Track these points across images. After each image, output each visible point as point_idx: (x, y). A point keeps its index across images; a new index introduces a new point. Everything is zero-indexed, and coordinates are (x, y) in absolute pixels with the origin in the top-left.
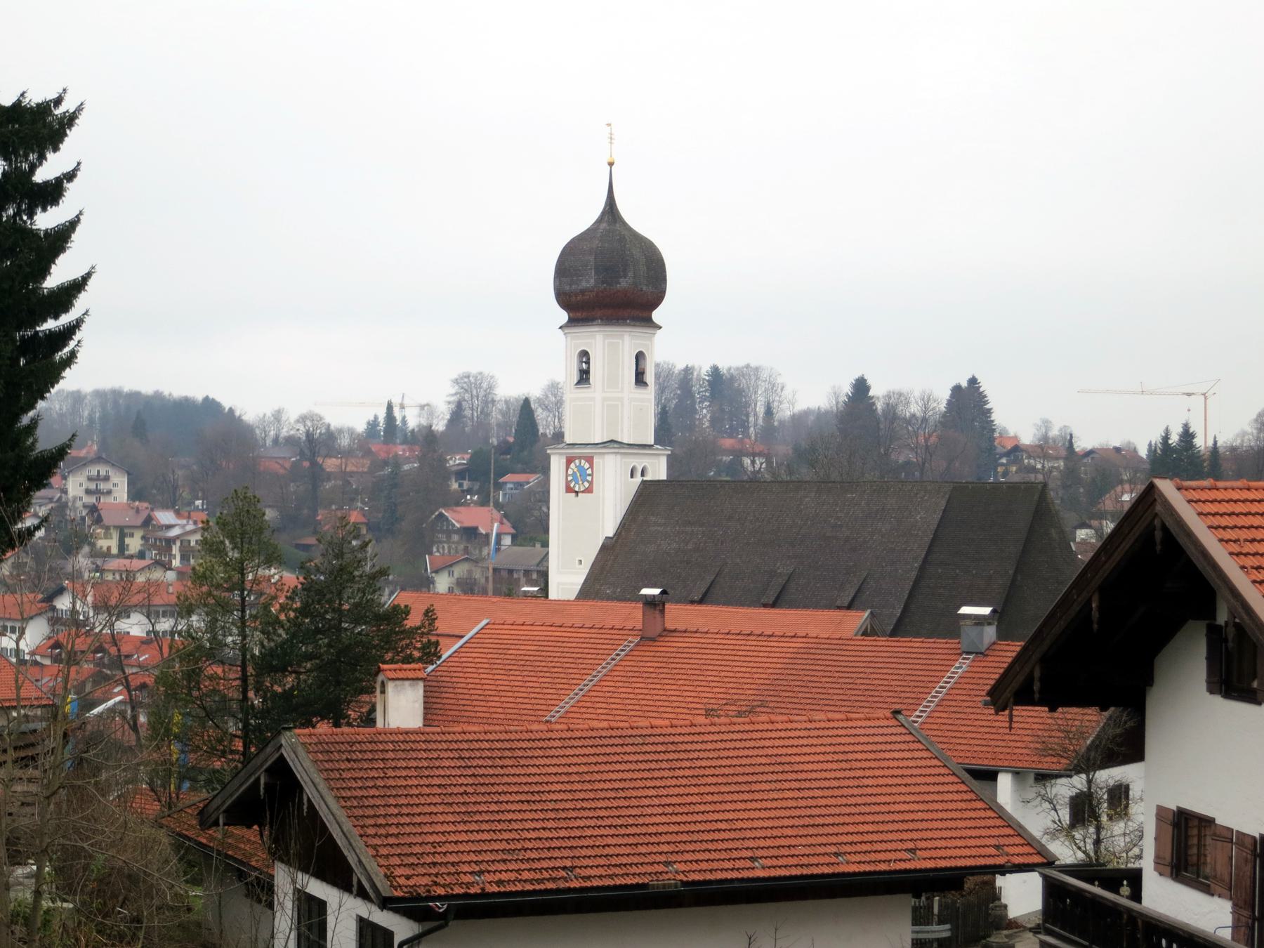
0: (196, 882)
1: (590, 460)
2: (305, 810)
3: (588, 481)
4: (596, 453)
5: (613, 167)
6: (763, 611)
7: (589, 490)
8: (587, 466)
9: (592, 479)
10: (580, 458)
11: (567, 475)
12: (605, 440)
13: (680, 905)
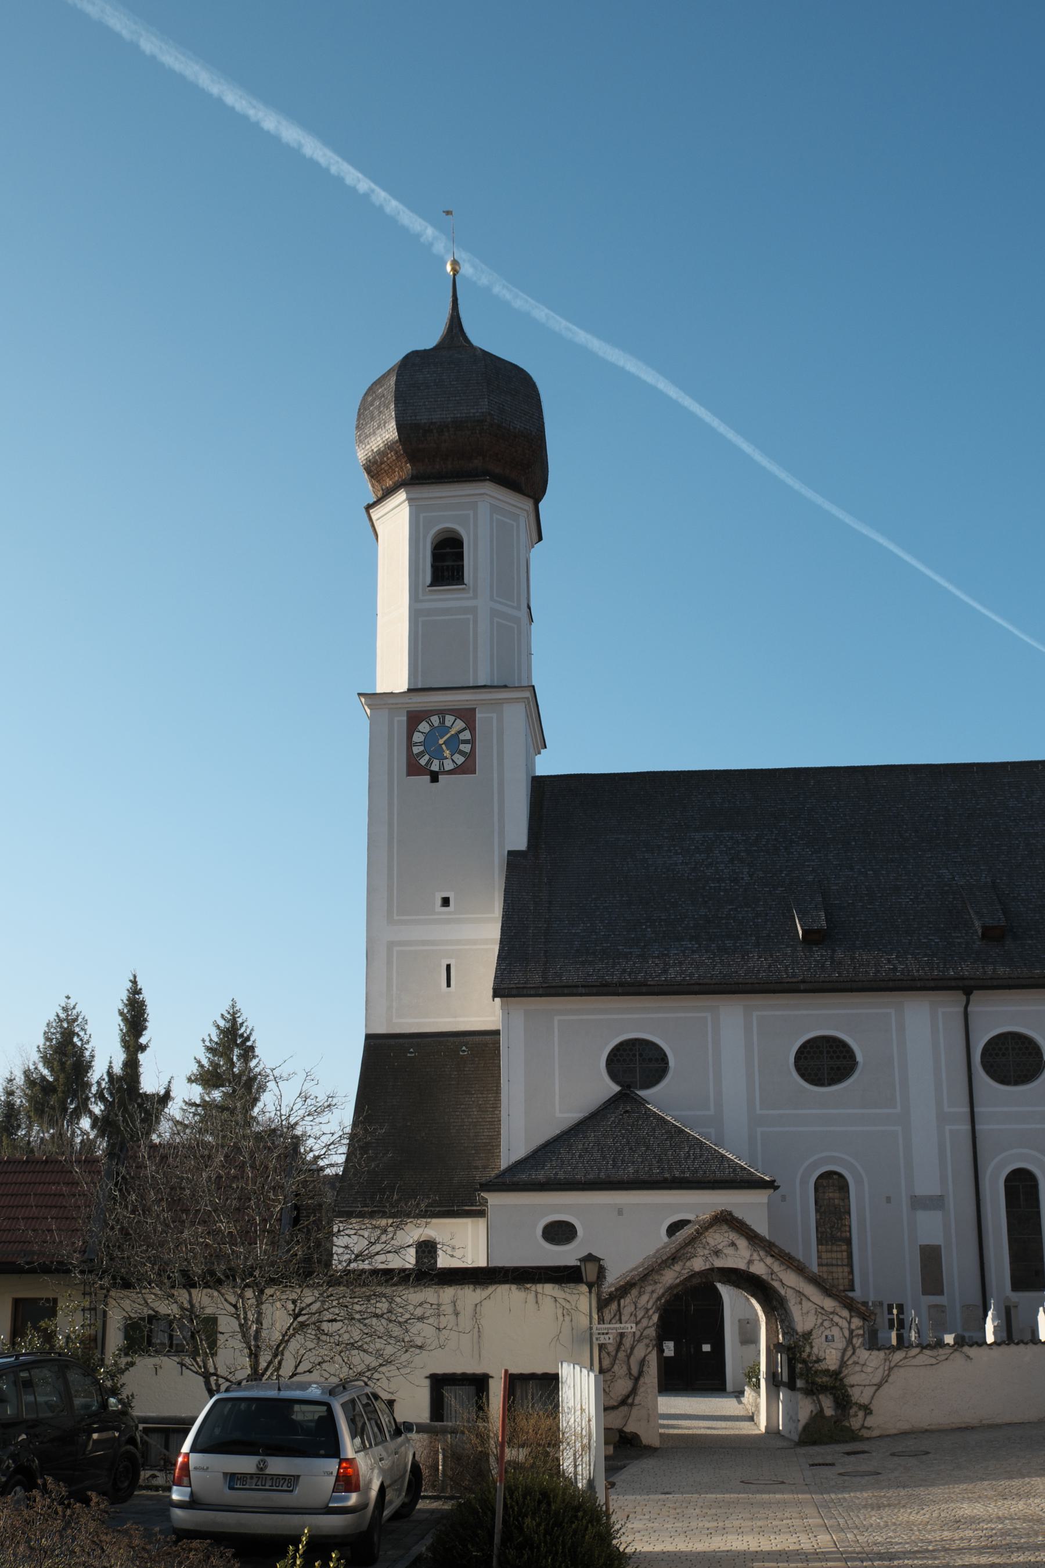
0: (481, 1452)
1: (468, 716)
3: (462, 753)
7: (467, 768)
9: (473, 749)
11: (410, 744)
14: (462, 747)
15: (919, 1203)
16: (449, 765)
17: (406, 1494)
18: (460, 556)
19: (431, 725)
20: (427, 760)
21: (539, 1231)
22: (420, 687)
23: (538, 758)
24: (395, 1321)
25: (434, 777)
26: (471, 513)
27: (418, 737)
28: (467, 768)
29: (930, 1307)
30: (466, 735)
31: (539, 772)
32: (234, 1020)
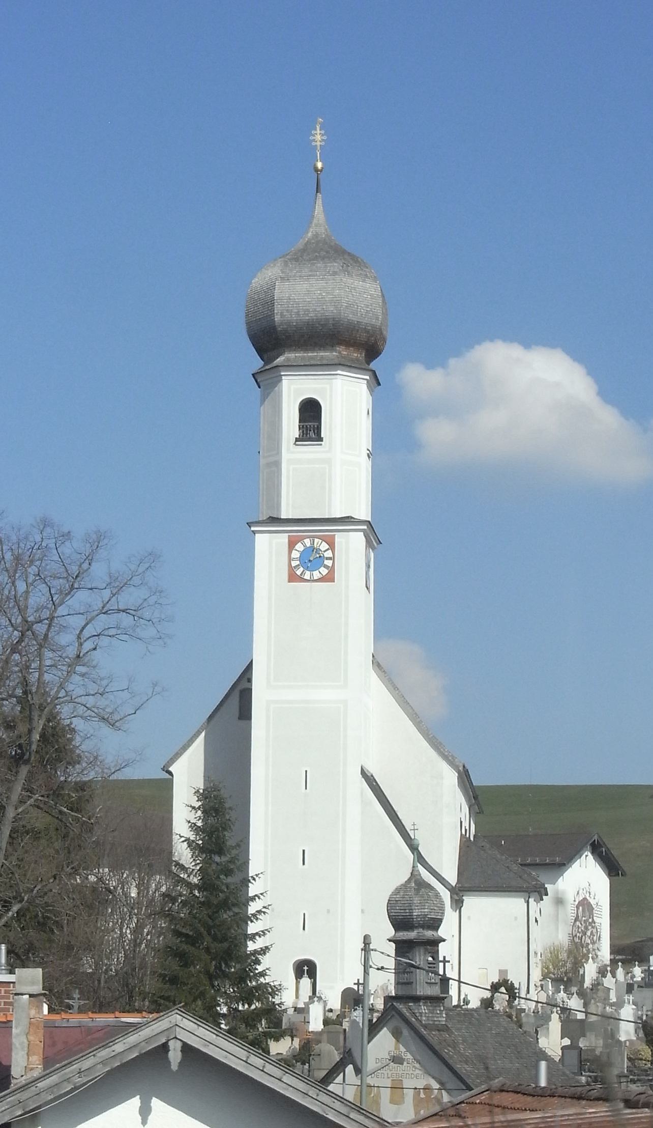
3: (326, 567)
7: (329, 578)
8: (324, 546)
11: (290, 559)
16: (316, 575)
20: (296, 564)
24: (80, 605)
27: (295, 554)
28: (329, 578)
30: (329, 554)
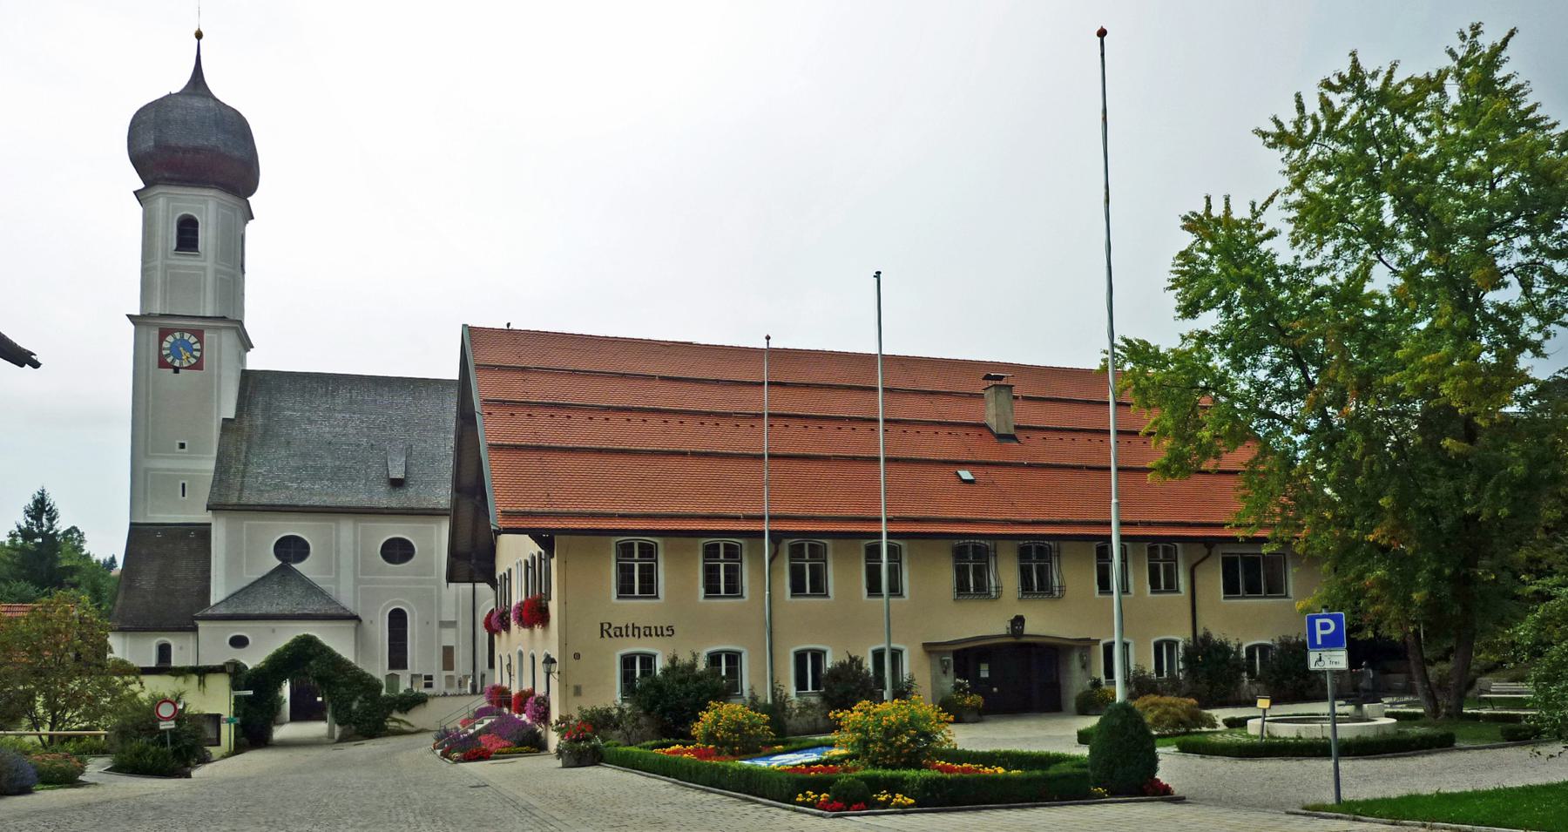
1: (198, 334)
2: (1258, 669)
3: (195, 357)
4: (209, 327)
5: (201, 41)
6: (246, 275)
7: (198, 366)
8: (193, 340)
9: (202, 355)
10: (182, 331)
11: (161, 349)
12: (217, 315)
13: (278, 619)
14: (195, 353)
15: (443, 624)
17: (1152, 588)
18: (196, 233)
19: (175, 338)
21: (228, 642)
22: (167, 313)
23: (248, 354)
25: (176, 370)
26: (204, 207)
27: (166, 345)
28: (198, 366)
29: (447, 677)
30: (197, 346)
31: (250, 366)
32: (43, 494)
